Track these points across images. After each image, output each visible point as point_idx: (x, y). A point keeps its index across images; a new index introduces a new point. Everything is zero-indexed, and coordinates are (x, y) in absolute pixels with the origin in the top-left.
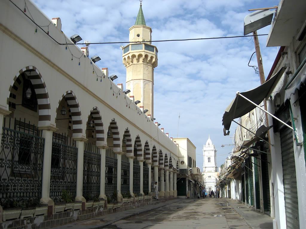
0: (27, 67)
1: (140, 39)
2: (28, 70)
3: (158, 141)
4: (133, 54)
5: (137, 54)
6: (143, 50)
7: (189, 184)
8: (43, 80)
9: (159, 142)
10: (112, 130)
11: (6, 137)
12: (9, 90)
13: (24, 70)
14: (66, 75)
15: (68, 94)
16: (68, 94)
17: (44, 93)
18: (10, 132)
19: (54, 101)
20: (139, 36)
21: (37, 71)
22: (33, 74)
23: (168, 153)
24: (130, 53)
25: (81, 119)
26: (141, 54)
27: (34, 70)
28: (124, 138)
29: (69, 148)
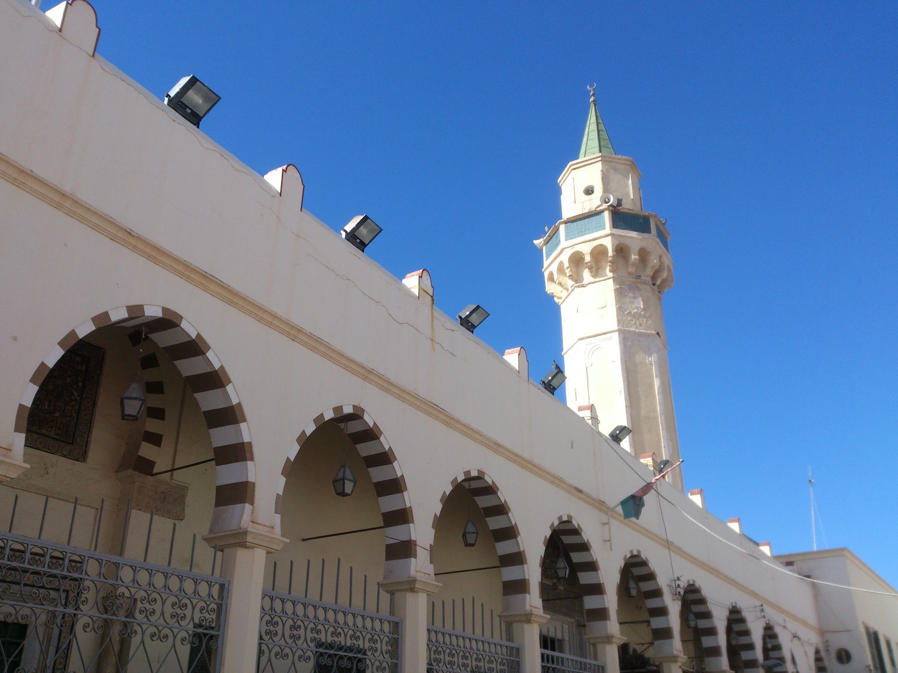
0: (130, 308)
1: (594, 202)
2: (469, 479)
3: (664, 536)
4: (573, 250)
5: (586, 249)
6: (608, 229)
7: (67, 656)
8: (388, 441)
9: (670, 539)
10: (487, 519)
11: (299, 627)
12: (283, 473)
13: (461, 478)
14: (334, 356)
15: (562, 522)
16: (562, 522)
17: (74, 343)
18: (207, 587)
19: (609, 576)
20: (592, 192)
21: (184, 325)
22: (354, 427)
23: (746, 604)
24: (562, 250)
25: (408, 506)
26: (601, 245)
27: (480, 478)
28: (765, 643)
29: (447, 637)
